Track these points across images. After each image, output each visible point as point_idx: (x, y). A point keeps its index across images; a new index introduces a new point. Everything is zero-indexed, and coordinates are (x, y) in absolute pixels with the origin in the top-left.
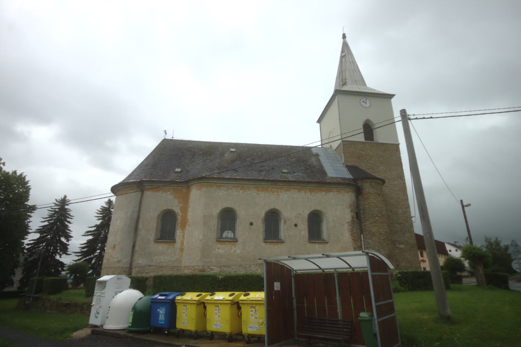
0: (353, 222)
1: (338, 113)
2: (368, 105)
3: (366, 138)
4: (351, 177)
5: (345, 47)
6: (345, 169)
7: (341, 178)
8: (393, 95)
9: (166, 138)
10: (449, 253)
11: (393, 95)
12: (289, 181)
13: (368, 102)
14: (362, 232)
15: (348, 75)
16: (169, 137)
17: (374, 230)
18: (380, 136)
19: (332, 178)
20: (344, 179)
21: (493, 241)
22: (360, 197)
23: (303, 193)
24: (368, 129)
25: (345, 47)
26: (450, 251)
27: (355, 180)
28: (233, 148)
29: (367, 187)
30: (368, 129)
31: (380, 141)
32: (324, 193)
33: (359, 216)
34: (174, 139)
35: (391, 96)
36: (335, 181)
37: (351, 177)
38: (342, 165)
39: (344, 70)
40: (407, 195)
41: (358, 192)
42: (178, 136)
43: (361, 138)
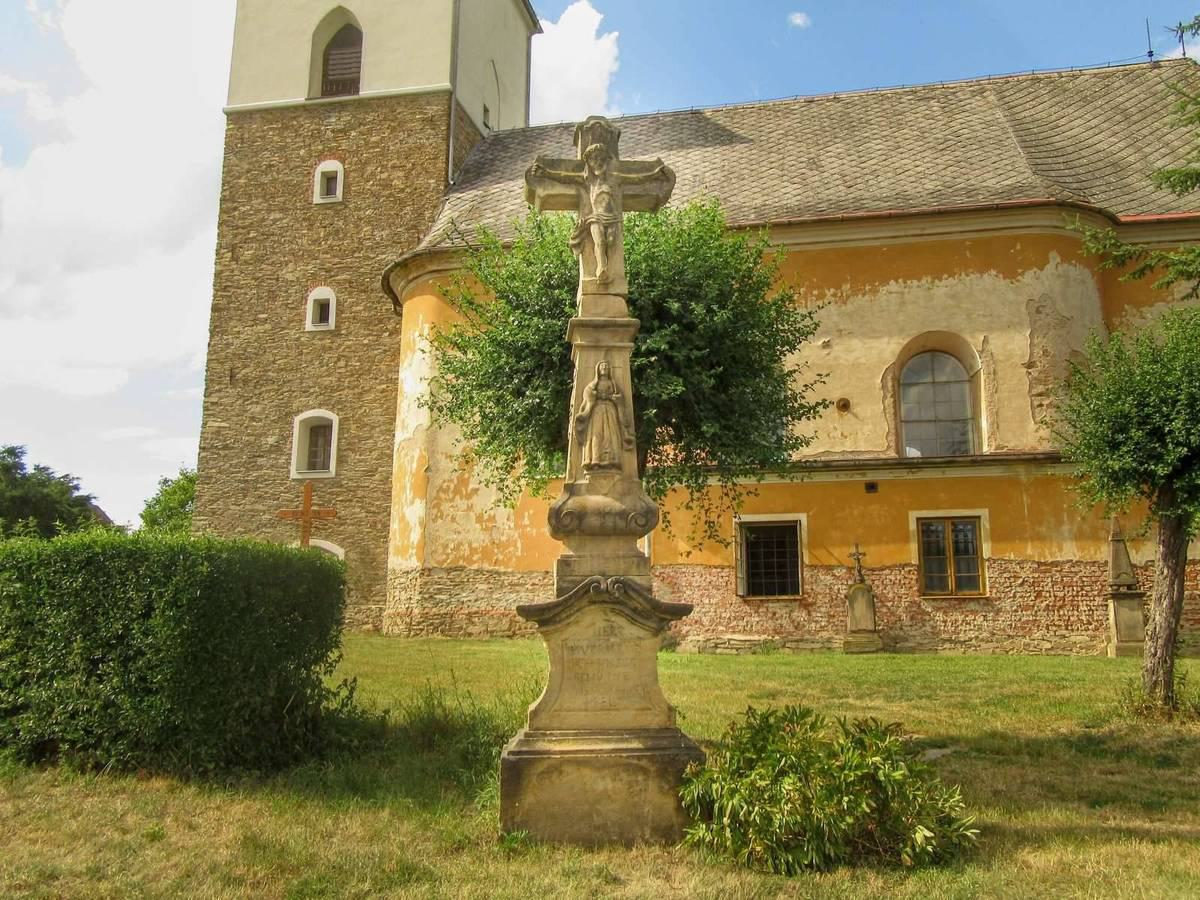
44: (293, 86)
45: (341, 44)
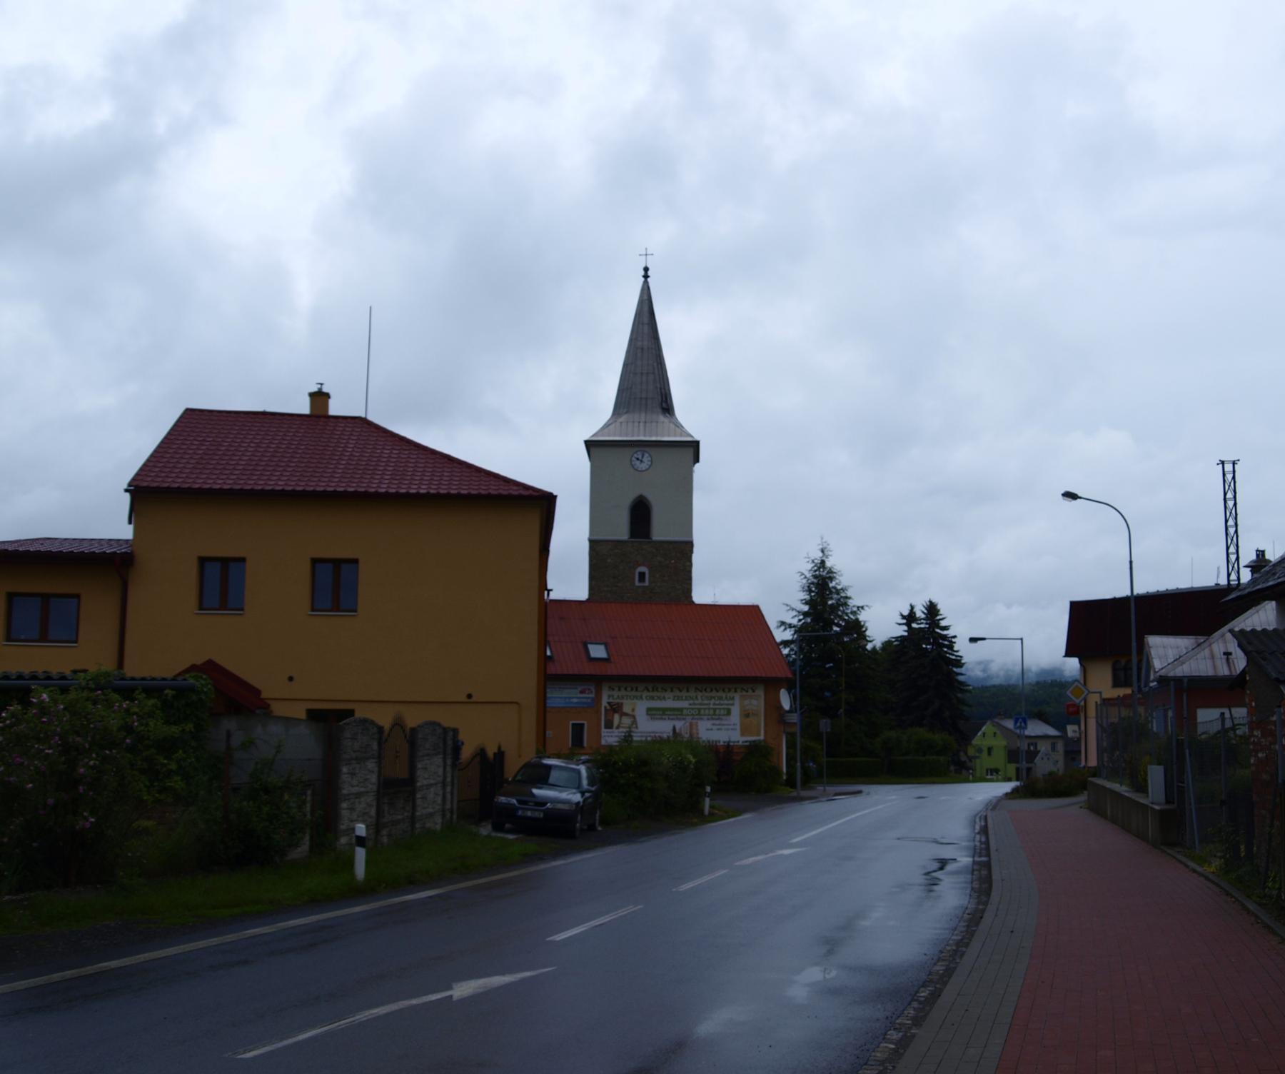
13: (646, 458)
44: (620, 530)
45: (641, 513)
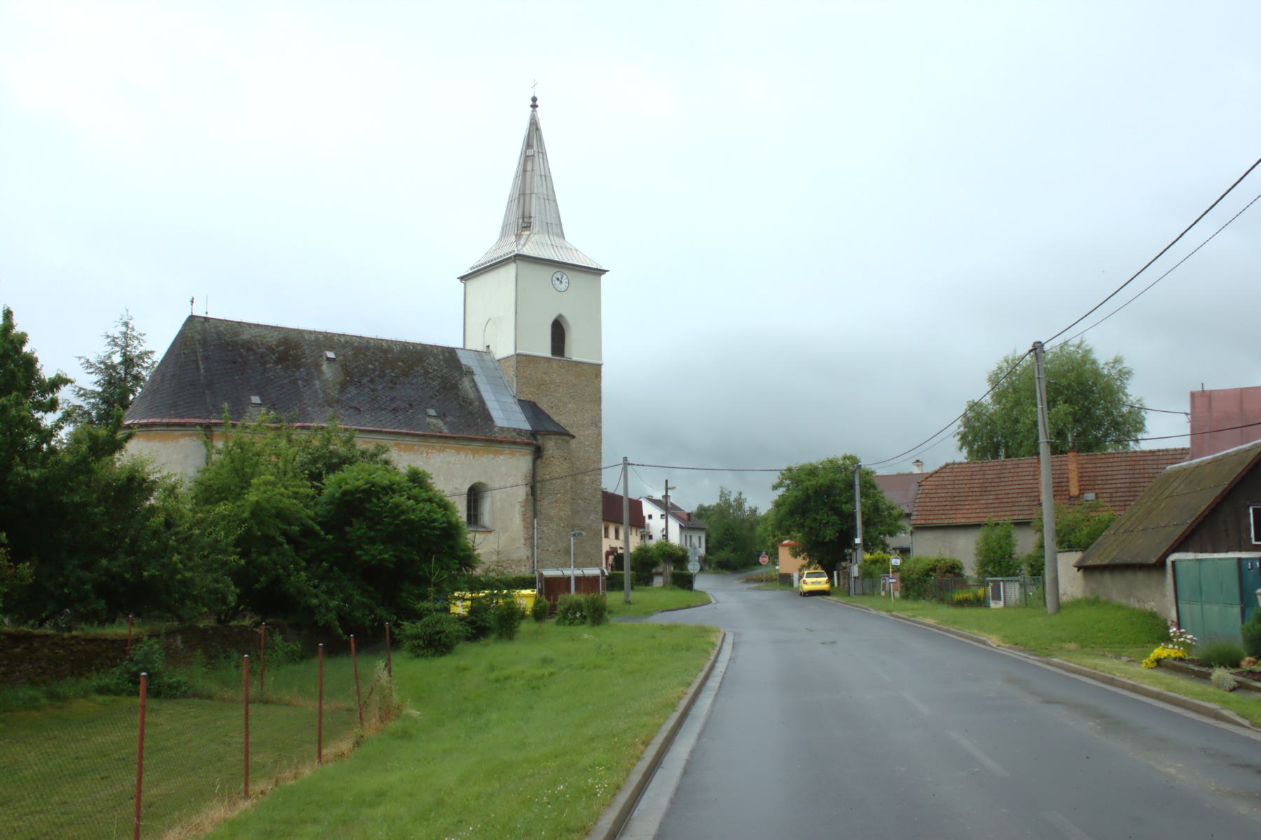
0: (527, 500)
1: (513, 310)
2: (562, 287)
3: (553, 353)
4: (526, 426)
5: (534, 127)
6: (517, 408)
7: (515, 430)
8: (605, 271)
9: (195, 314)
10: (647, 520)
11: (605, 271)
12: (446, 437)
14: (535, 515)
15: (535, 207)
16: (199, 312)
17: (553, 512)
18: (576, 350)
19: (501, 428)
20: (519, 432)
21: (732, 499)
22: (539, 462)
23: (462, 456)
24: (559, 331)
25: (534, 127)
26: (650, 517)
27: (534, 434)
28: (331, 349)
29: (551, 446)
30: (559, 331)
31: (574, 358)
32: (492, 456)
33: (534, 486)
34: (209, 316)
35: (600, 272)
36: (509, 436)
37: (526, 426)
38: (511, 400)
39: (528, 192)
40: (600, 453)
41: (538, 453)
42: (214, 314)
43: (544, 350)
